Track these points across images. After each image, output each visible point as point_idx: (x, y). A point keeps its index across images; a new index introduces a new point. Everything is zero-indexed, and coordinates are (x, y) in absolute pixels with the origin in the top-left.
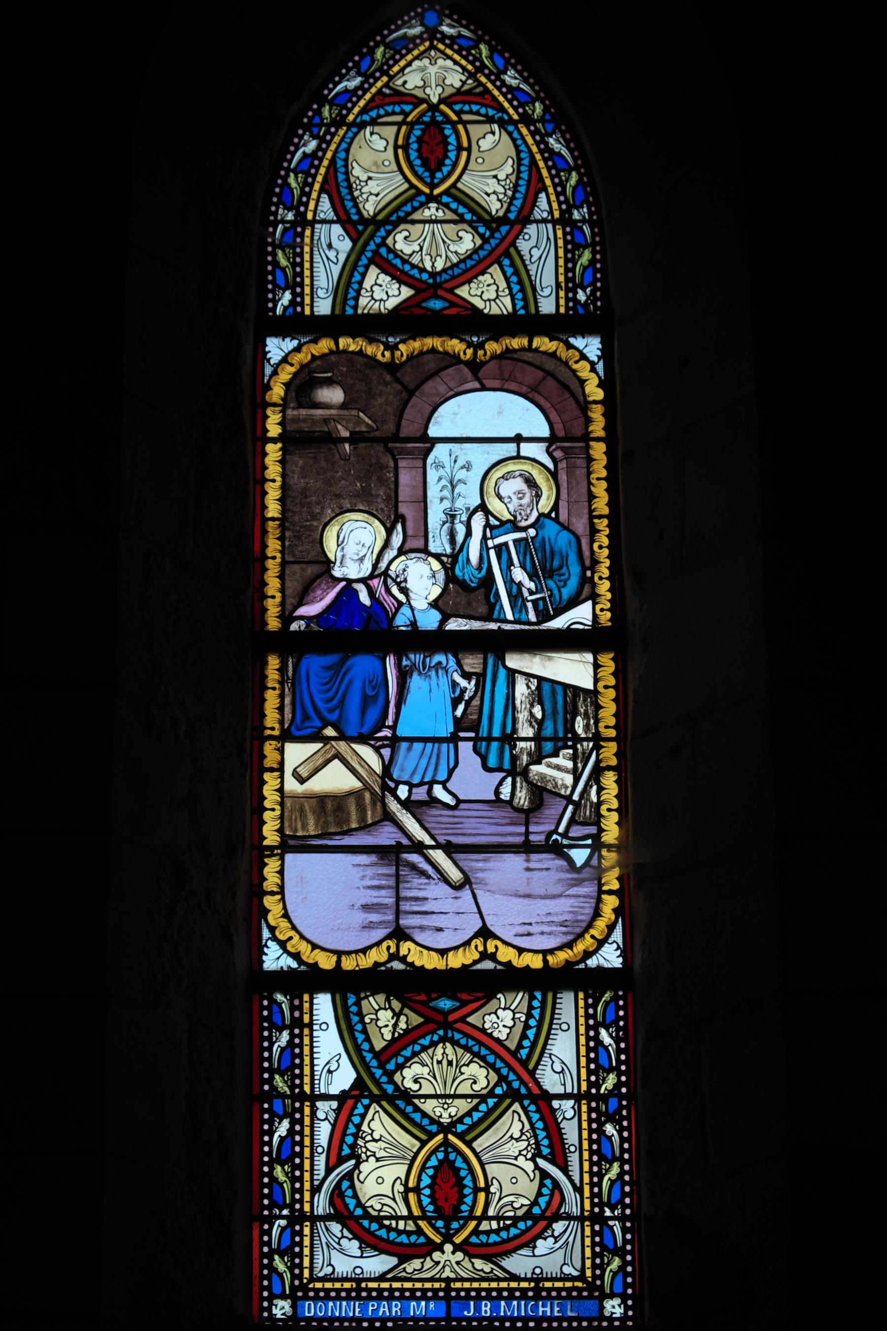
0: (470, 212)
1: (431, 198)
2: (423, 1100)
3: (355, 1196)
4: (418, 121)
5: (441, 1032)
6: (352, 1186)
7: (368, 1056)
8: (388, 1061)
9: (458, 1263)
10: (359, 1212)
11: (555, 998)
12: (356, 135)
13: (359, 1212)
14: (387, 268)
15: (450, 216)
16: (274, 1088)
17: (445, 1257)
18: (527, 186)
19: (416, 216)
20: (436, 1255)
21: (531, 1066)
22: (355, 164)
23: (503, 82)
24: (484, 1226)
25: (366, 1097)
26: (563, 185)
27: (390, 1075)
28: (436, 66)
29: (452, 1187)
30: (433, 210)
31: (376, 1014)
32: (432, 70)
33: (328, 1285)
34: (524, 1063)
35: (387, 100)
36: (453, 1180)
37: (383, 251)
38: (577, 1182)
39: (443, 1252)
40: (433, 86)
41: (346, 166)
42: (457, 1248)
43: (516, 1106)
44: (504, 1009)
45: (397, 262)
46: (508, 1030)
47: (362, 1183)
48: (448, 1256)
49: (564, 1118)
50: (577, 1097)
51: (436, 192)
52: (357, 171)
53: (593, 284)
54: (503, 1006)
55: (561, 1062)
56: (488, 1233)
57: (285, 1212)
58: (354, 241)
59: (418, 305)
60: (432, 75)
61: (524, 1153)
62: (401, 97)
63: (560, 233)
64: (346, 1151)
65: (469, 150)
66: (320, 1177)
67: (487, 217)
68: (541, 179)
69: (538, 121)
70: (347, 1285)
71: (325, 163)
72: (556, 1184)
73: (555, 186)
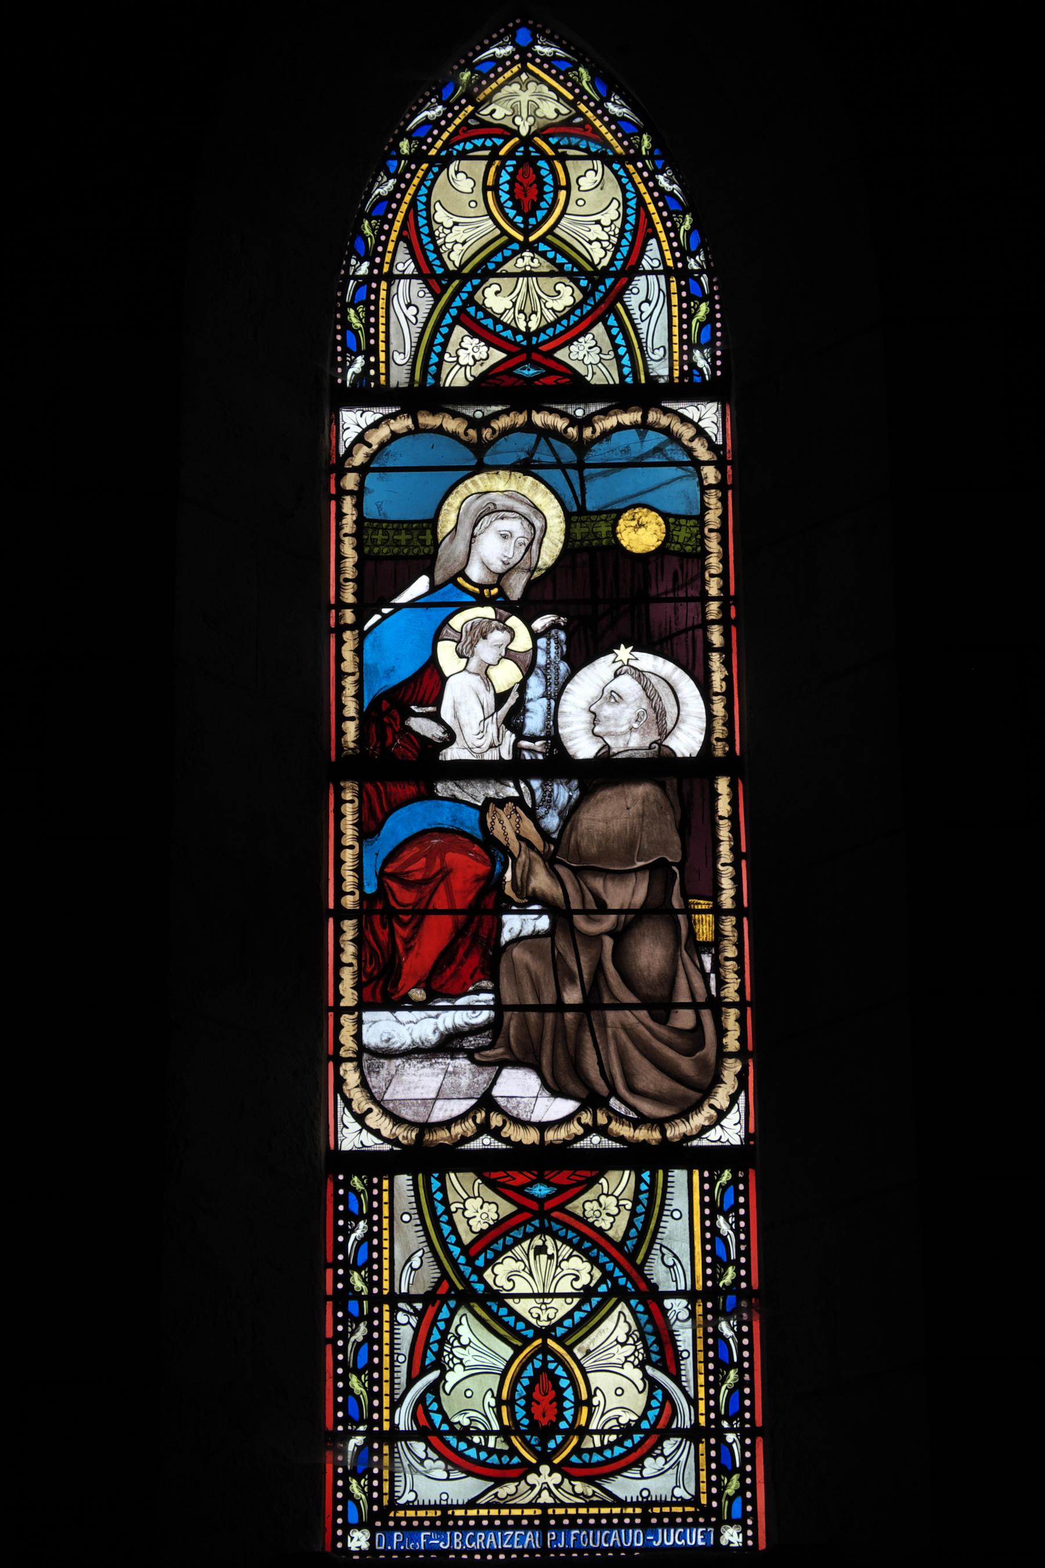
0: (569, 265)
1: (526, 246)
2: (517, 1300)
3: (441, 1410)
4: (511, 155)
5: (536, 1223)
6: (438, 1399)
7: (456, 1251)
8: (477, 1257)
9: (557, 1486)
10: (445, 1427)
11: (666, 1176)
12: (437, 175)
13: (445, 1427)
14: (476, 331)
15: (546, 267)
16: (349, 1286)
17: (542, 1479)
18: (637, 232)
19: (509, 267)
20: (532, 1478)
21: (639, 1261)
22: (438, 206)
23: (606, 112)
24: (587, 1444)
25: (452, 1297)
26: (675, 229)
27: (479, 1272)
28: (529, 93)
29: (551, 1403)
30: (527, 260)
31: (464, 1204)
32: (524, 97)
33: (411, 1513)
34: (632, 1256)
35: (472, 133)
36: (552, 1394)
37: (472, 310)
38: (691, 1393)
39: (539, 1474)
40: (524, 115)
41: (428, 209)
42: (554, 1469)
43: (622, 1307)
44: (607, 1195)
45: (489, 323)
46: (463, 344)
47: (449, 1395)
48: (546, 1477)
49: (677, 1319)
50: (691, 1296)
51: (532, 238)
52: (440, 216)
53: (711, 344)
54: (468, 368)
55: (676, 1257)
56: (590, 1451)
57: (362, 1428)
58: (437, 298)
59: (561, 1189)
60: (525, 102)
61: (632, 1359)
62: (490, 129)
63: (674, 286)
64: (430, 1358)
65: (568, 188)
66: (401, 1392)
67: (589, 269)
68: (651, 224)
69: (646, 157)
70: (431, 1513)
71: (404, 207)
72: (667, 1395)
73: (667, 231)
